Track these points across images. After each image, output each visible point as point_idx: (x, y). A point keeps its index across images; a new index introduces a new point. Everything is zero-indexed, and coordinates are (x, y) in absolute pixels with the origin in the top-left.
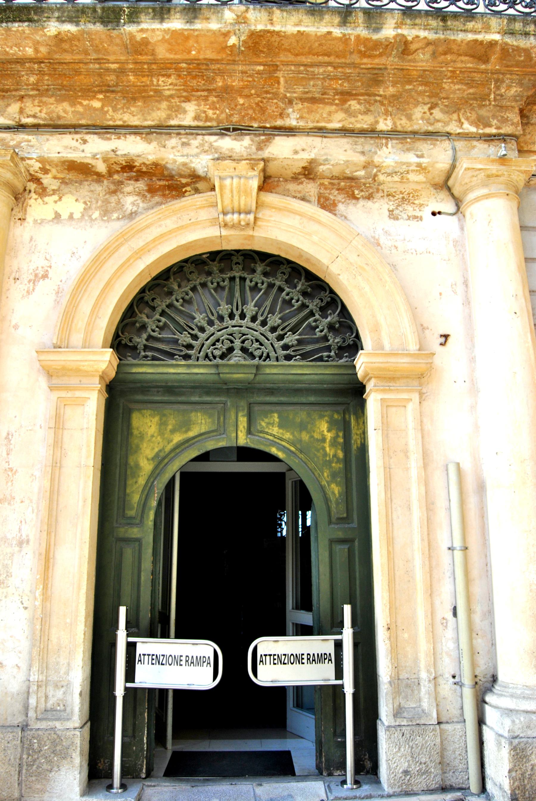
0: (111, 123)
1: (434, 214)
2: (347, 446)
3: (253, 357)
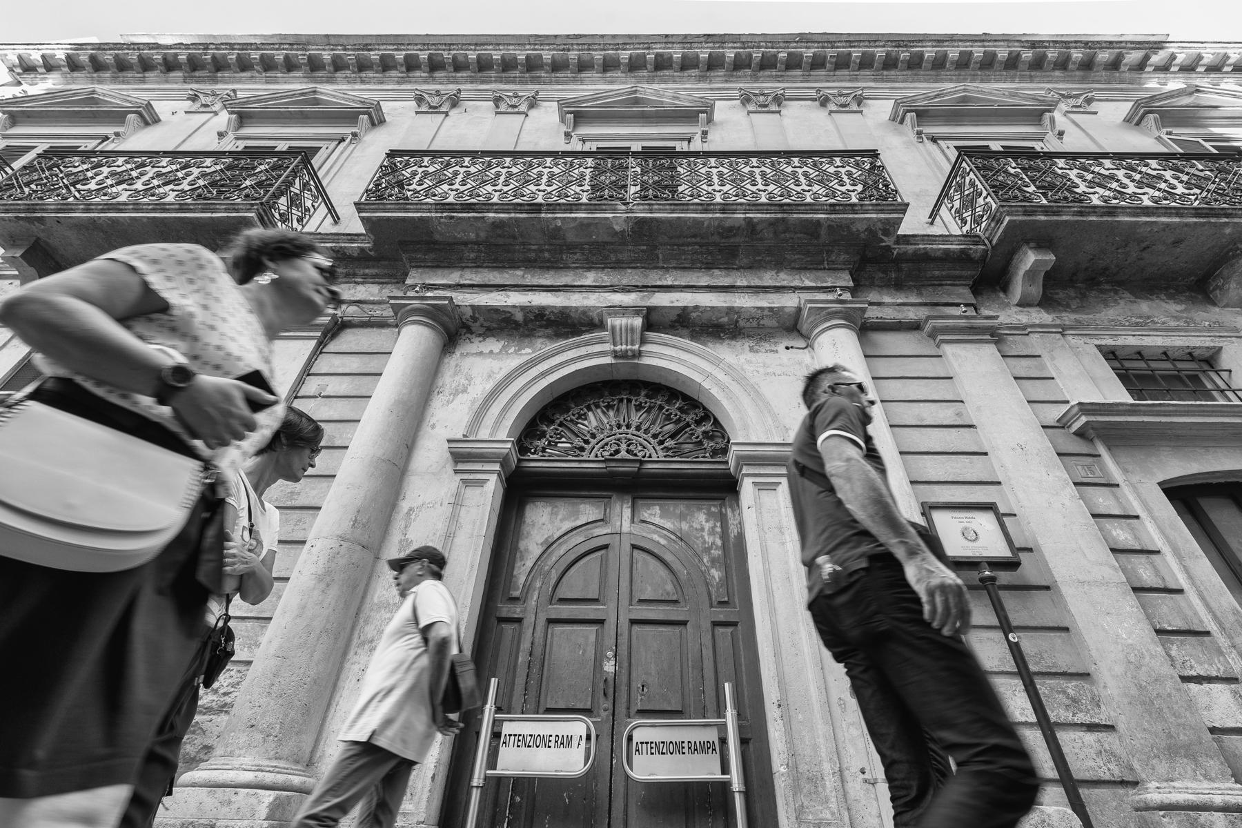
1: (787, 348)
2: (724, 535)
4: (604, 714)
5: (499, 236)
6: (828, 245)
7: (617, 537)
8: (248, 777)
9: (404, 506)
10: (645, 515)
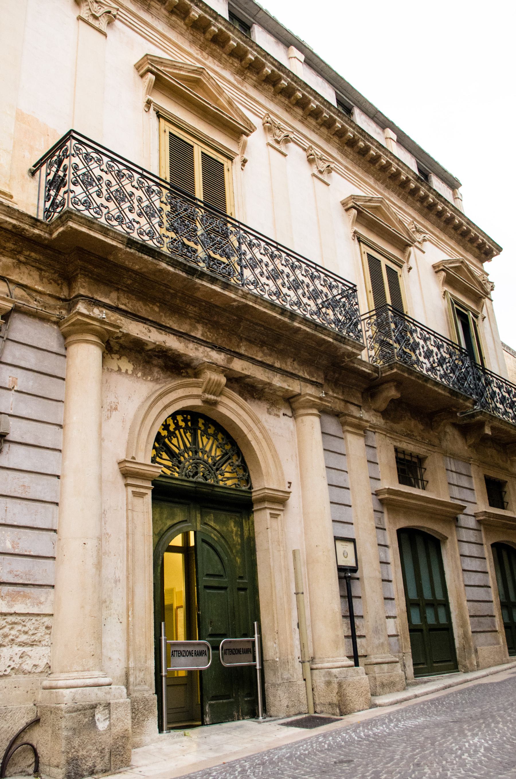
0: (164, 324)
1: (284, 415)
2: (242, 536)
10: (207, 520)
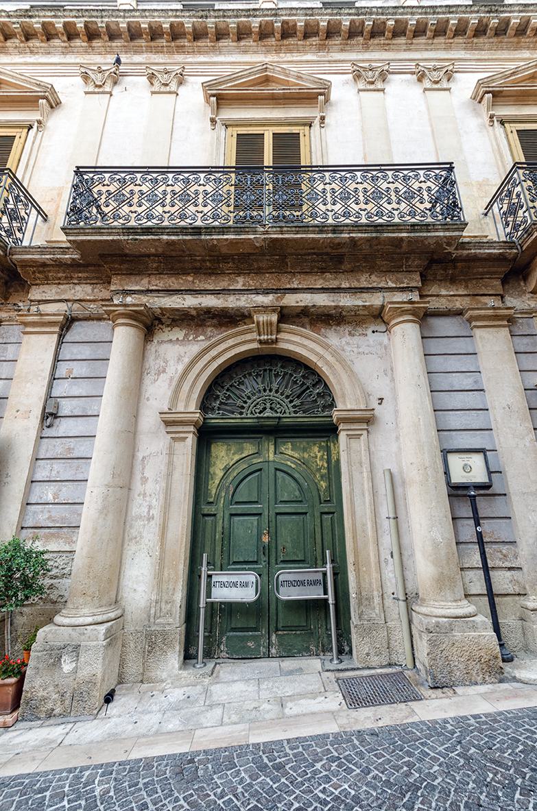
1: (373, 332)
2: (329, 461)
3: (277, 412)
4: (264, 564)
5: (172, 250)
6: (407, 253)
7: (267, 463)
8: (90, 620)
9: (140, 455)
